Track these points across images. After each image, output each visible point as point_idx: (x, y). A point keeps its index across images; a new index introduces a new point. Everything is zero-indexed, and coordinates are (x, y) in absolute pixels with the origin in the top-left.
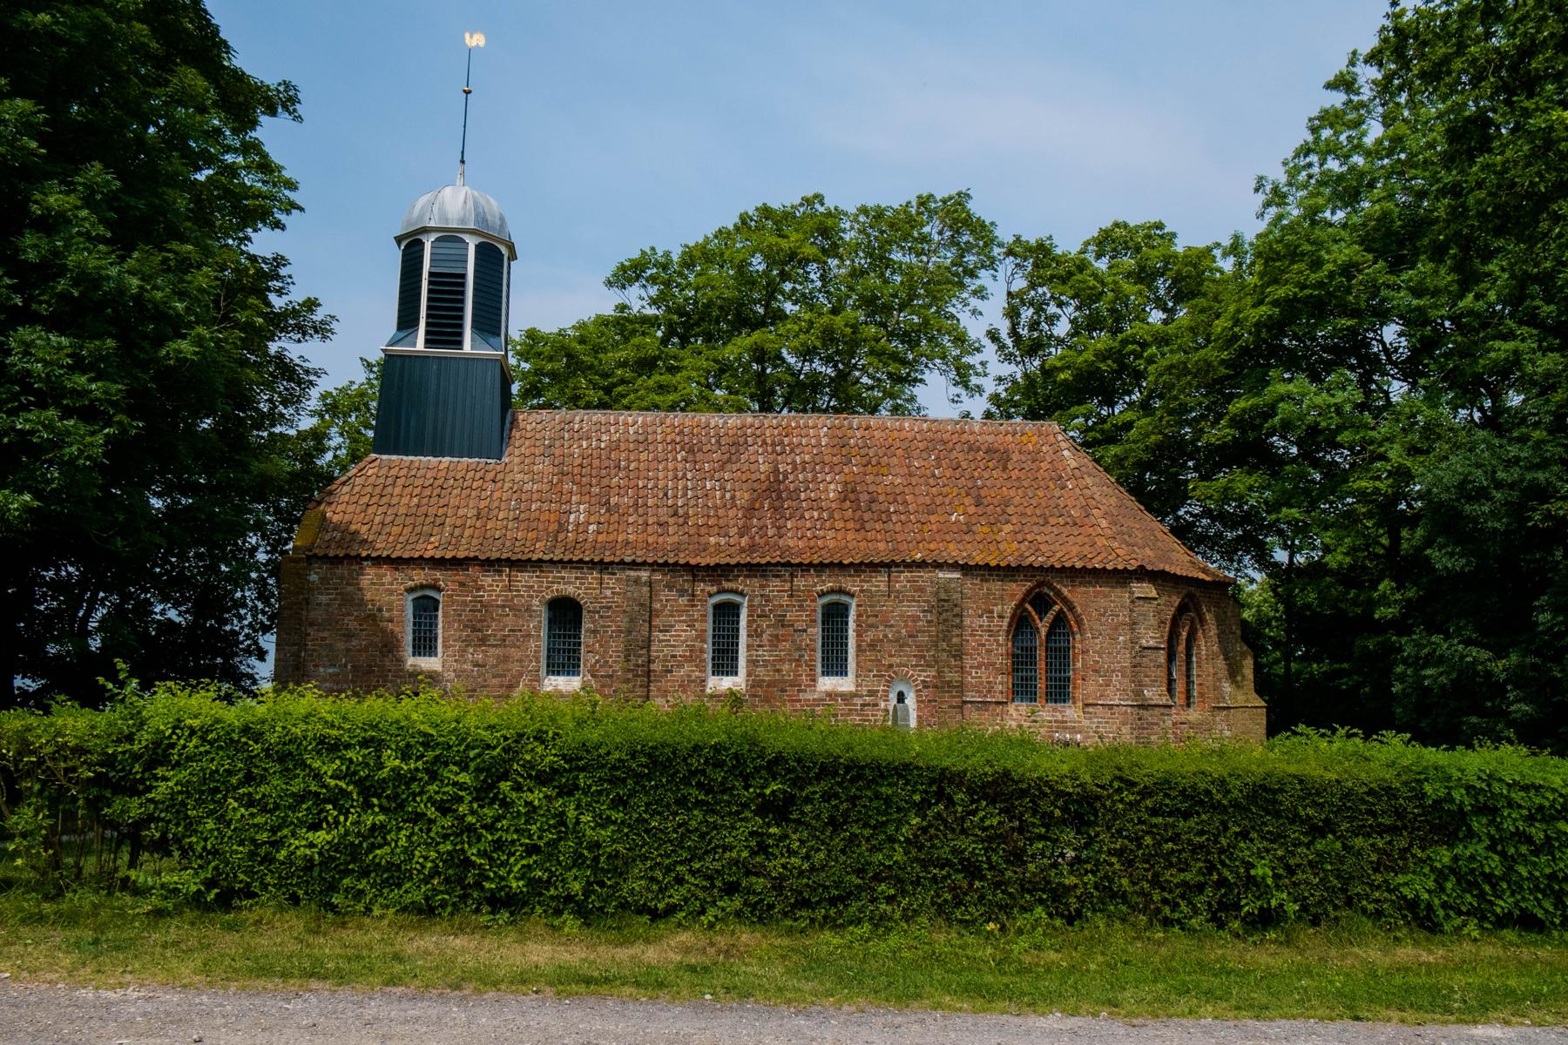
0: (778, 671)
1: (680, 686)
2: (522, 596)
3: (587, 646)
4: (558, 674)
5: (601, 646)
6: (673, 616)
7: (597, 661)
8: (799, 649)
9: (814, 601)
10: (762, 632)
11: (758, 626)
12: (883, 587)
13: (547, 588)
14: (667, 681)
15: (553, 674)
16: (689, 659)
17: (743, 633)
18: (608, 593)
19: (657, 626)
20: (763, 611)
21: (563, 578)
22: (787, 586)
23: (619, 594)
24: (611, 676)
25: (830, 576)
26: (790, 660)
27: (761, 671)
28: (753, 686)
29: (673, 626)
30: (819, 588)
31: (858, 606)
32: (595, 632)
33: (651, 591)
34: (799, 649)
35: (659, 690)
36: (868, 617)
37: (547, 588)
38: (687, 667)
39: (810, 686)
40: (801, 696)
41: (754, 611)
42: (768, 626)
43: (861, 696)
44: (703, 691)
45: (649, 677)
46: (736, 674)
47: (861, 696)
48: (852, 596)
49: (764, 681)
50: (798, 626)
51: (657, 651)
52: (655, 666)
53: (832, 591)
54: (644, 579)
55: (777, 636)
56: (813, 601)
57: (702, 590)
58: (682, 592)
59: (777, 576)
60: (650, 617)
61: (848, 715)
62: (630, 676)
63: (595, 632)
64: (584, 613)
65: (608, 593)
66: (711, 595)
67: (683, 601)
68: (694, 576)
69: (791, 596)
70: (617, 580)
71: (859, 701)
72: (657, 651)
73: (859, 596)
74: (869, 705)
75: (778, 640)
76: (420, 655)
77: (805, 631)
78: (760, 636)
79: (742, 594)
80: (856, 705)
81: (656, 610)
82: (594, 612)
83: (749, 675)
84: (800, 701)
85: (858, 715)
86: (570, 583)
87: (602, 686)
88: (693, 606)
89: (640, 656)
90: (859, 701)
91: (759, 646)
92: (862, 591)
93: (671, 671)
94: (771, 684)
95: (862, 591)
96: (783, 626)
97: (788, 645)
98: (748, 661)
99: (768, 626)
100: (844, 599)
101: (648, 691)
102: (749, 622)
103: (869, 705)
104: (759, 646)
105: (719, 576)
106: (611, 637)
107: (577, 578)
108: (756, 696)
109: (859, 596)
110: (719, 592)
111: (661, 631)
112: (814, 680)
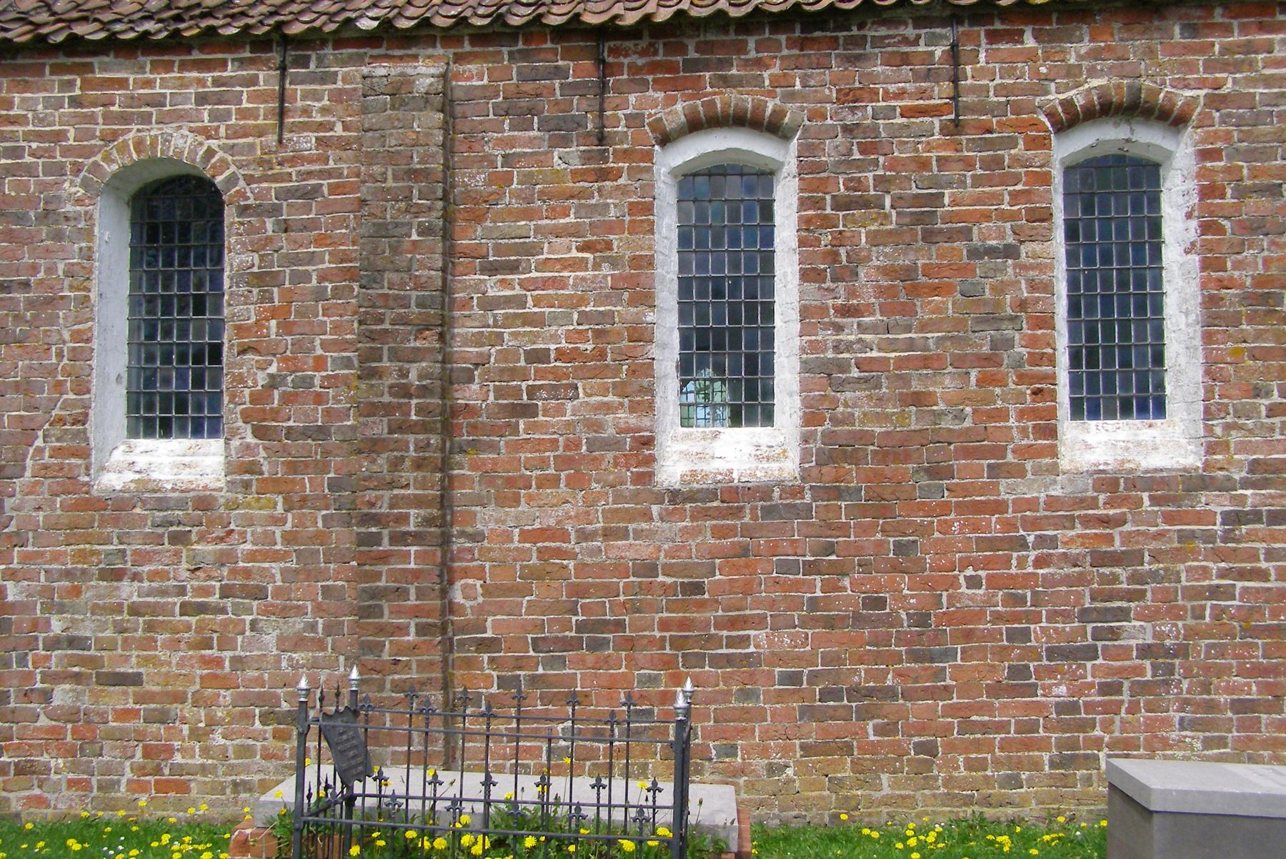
0: (918, 399)
1: (563, 463)
2: (30, 170)
3: (240, 330)
4: (166, 431)
5: (286, 327)
6: (529, 215)
7: (274, 382)
8: (992, 318)
9: (1041, 143)
10: (856, 260)
11: (839, 239)
12: (718, 399)
13: (109, 138)
14: (517, 446)
15: (149, 433)
16: (594, 365)
17: (787, 267)
18: (307, 142)
19: (472, 254)
20: (857, 184)
21: (158, 102)
22: (940, 92)
23: (344, 144)
24: (322, 432)
25: (1095, 55)
26: (958, 362)
27: (855, 403)
28: (825, 459)
29: (533, 250)
30: (1054, 98)
31: (1205, 155)
32: (263, 279)
33: (446, 127)
34: (992, 318)
35: (488, 477)
36: (1241, 193)
37: (109, 138)
38: (587, 396)
39: (1027, 452)
40: (1007, 490)
41: (822, 185)
42: (875, 239)
43: (1226, 486)
44: (646, 478)
45: (447, 429)
46: (1160, 411)
47: (1226, 486)
48: (1174, 120)
49: (866, 437)
50: (990, 234)
51: (478, 340)
52: (470, 394)
53: (1104, 110)
54: (423, 84)
55: (908, 273)
56: (1033, 143)
57: (635, 120)
58: (561, 131)
59: (905, 59)
60: (448, 218)
61: (1179, 555)
62: (379, 428)
63: (263, 279)
64: (230, 215)
65: (307, 142)
66: (666, 140)
67: (567, 158)
68: (605, 69)
69: (955, 127)
70: (337, 96)
71: (1218, 504)
72: (478, 340)
73: (1204, 122)
74: (1256, 516)
75: (915, 290)
76: (1094, 414)
77: (1010, 252)
78: (847, 274)
79: (774, 128)
80: (1208, 517)
81: (471, 197)
82: (261, 211)
83: (811, 418)
84: (1000, 507)
85: (1218, 555)
86: (180, 116)
87: (293, 468)
88: (603, 175)
89: (415, 356)
90: (1218, 504)
91: (846, 311)
92: (1217, 101)
93: (529, 411)
94: (894, 450)
95: (1217, 101)
96: (929, 237)
97: (949, 304)
98: (807, 367)
99: (875, 239)
100: (1147, 137)
101: (447, 486)
102: (806, 225)
103: (1256, 516)
104: (846, 311)
105: (692, 66)
106: (319, 295)
107: (202, 99)
108: (838, 494)
109: (1204, 122)
110: (695, 125)
111: (492, 269)
112: (1051, 432)
